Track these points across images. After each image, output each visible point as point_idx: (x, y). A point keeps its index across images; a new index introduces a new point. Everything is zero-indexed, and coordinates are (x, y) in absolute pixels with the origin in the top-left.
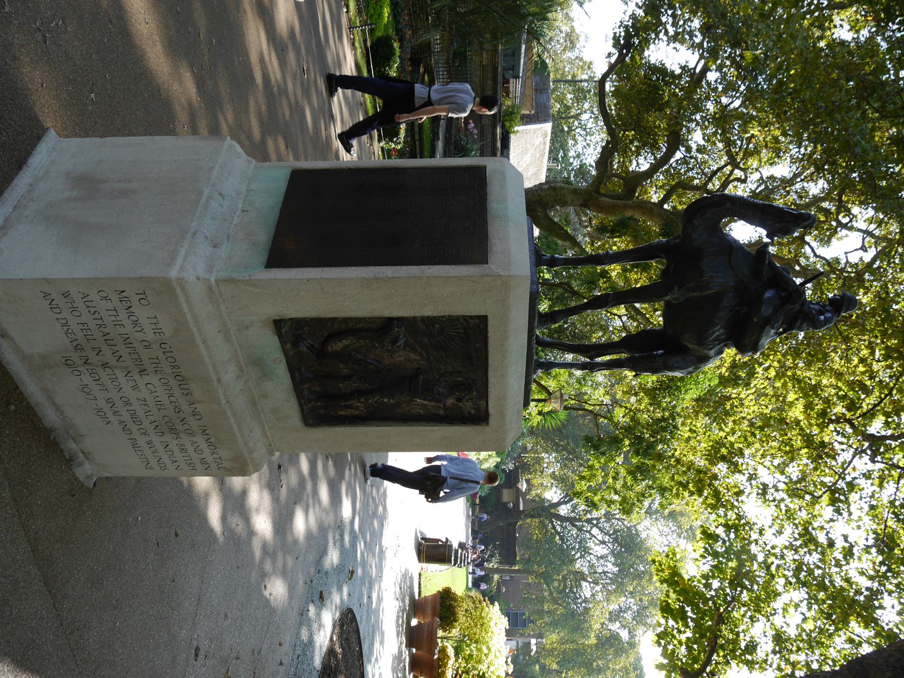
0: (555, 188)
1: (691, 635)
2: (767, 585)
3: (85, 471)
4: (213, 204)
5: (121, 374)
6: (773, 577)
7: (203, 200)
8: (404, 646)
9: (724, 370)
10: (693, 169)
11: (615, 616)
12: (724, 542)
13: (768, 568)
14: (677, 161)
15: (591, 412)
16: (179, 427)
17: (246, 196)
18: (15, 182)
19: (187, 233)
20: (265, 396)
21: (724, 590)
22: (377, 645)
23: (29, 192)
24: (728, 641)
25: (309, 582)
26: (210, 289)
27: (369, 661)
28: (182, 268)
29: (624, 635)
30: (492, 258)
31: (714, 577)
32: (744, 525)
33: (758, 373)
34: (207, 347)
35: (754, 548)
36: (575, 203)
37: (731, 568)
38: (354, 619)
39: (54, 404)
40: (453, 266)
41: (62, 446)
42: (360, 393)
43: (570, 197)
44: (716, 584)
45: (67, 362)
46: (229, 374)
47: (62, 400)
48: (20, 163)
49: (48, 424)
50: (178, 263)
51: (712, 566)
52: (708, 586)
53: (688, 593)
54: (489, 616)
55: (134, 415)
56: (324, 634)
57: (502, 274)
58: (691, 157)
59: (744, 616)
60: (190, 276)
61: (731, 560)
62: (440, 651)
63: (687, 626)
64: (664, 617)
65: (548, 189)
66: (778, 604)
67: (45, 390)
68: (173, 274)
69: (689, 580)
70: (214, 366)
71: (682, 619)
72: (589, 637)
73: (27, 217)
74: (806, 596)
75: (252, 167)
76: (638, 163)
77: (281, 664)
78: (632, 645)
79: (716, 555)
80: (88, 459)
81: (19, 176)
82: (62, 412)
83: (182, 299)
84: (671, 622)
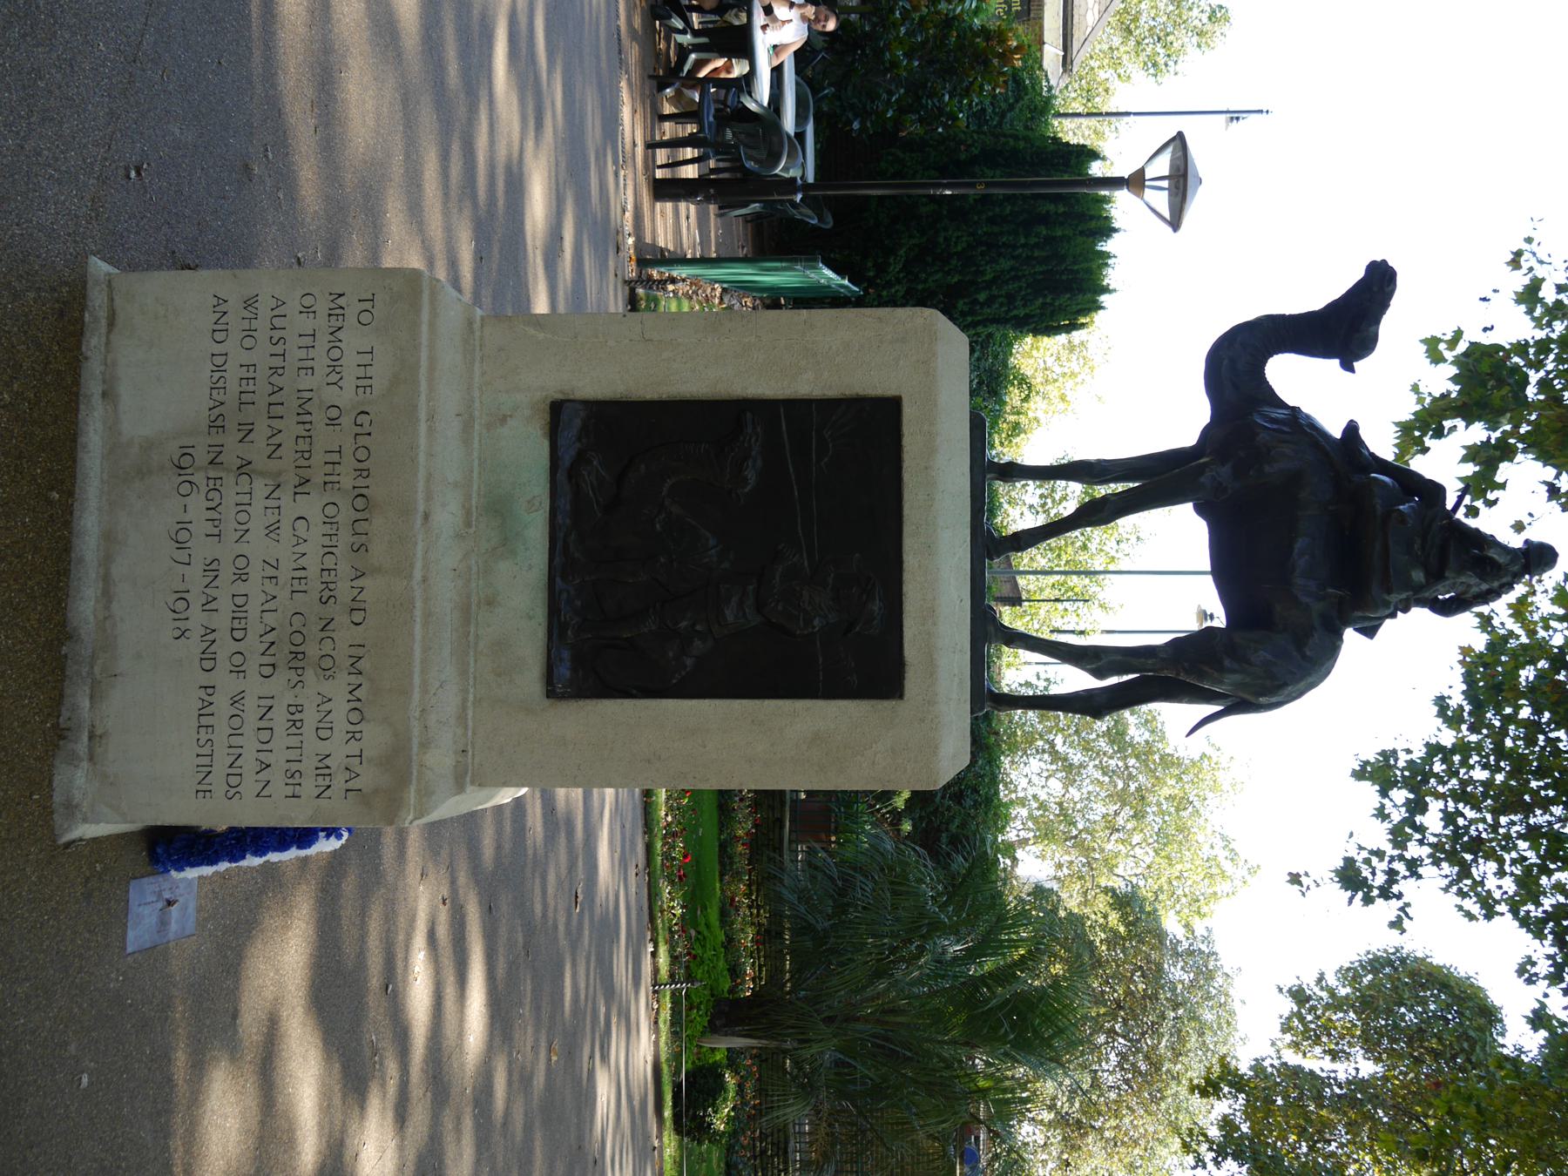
34: (431, 430)
46: (448, 515)
67: (109, 537)
80: (91, 758)
83: (425, 316)
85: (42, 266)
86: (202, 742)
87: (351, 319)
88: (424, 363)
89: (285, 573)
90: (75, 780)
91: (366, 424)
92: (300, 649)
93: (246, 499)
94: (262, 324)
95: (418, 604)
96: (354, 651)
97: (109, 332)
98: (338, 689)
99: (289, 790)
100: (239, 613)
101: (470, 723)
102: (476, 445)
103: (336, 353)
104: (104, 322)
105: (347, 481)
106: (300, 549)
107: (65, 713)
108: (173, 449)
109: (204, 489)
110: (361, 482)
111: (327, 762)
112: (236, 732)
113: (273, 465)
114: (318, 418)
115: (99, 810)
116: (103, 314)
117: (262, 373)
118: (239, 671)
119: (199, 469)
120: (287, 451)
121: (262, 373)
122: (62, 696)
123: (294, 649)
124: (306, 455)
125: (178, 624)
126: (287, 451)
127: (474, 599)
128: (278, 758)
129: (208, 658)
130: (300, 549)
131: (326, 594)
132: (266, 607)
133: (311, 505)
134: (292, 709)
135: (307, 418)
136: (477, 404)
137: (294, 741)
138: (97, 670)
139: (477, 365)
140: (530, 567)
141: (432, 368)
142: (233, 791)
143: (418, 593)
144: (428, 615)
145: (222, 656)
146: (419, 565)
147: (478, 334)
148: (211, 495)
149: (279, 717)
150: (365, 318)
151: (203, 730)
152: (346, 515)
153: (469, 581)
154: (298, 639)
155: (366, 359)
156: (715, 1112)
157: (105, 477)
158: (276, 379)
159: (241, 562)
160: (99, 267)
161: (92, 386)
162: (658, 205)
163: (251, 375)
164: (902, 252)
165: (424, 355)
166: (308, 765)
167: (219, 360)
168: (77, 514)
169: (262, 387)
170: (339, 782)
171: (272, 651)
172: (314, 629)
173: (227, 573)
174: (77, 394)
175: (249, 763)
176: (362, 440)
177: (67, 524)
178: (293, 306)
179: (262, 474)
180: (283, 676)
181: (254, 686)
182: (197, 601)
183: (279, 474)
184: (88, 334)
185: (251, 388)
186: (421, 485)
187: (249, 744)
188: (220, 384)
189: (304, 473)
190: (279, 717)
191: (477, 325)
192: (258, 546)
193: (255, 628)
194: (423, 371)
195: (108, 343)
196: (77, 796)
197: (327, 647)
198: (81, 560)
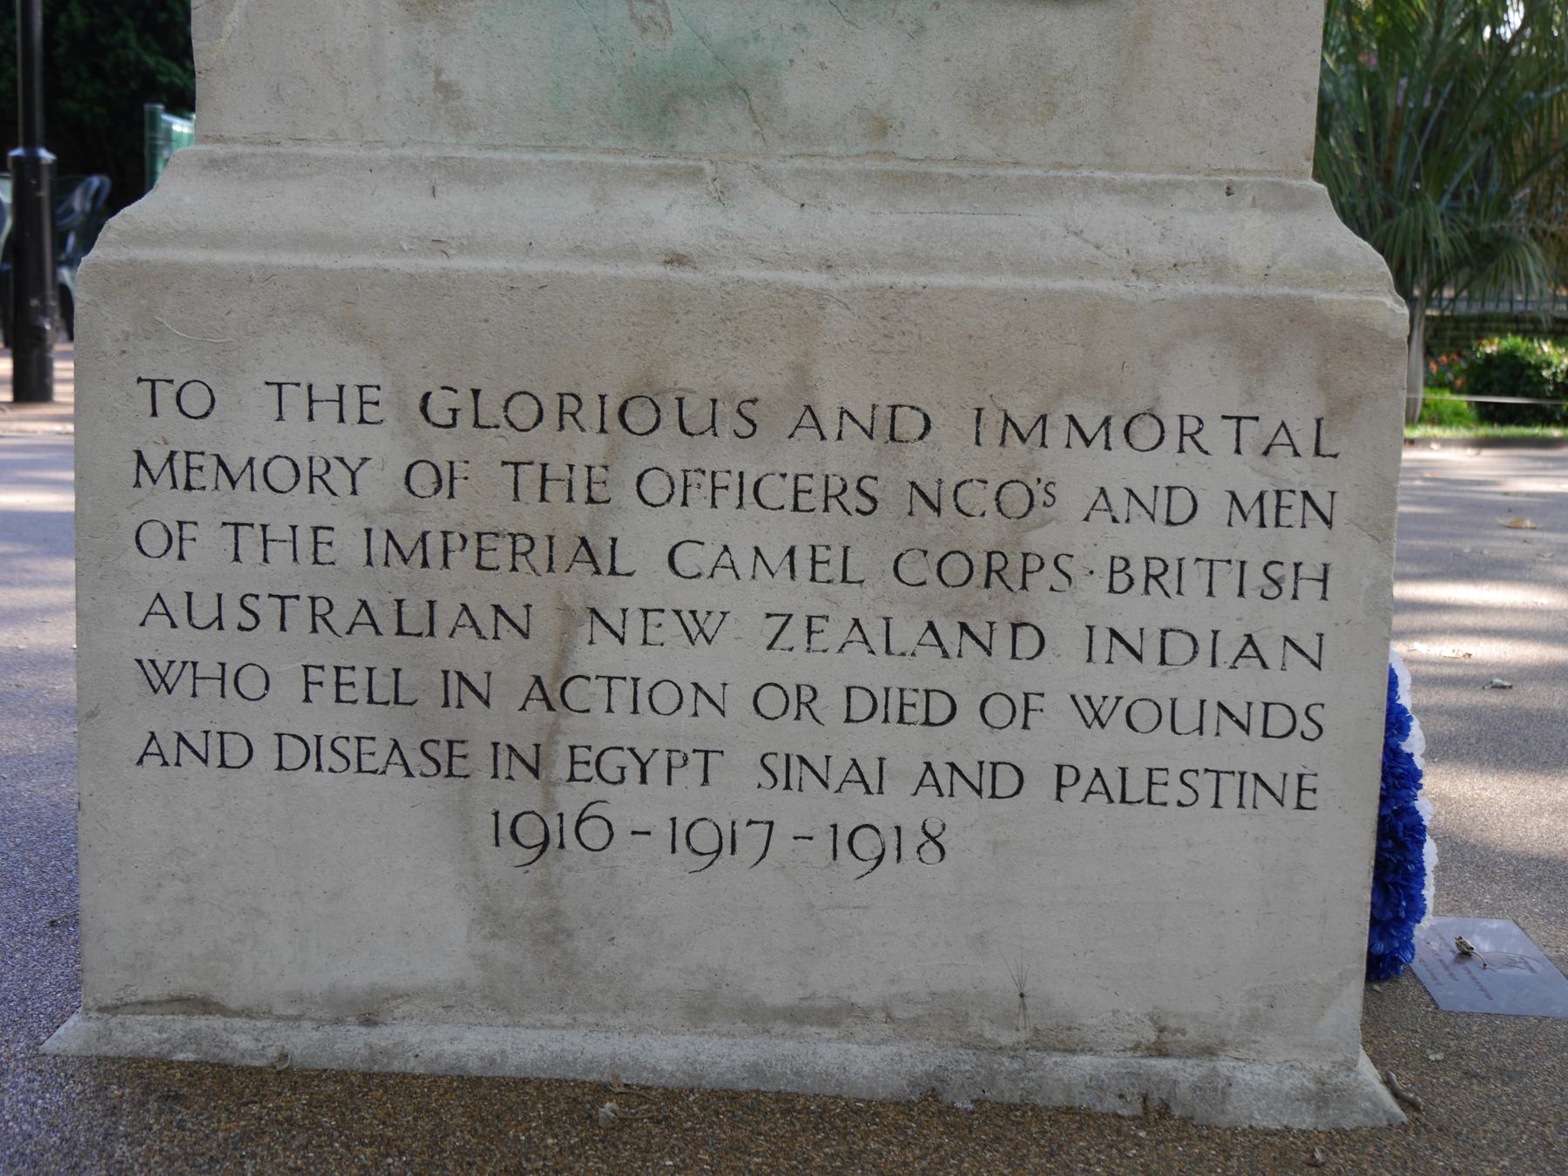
34: (469, 246)
46: (675, 217)
67: (701, 1011)
85: (53, 1127)
86: (1188, 797)
87: (199, 435)
88: (307, 259)
89: (801, 597)
90: (1264, 1083)
91: (453, 400)
92: (980, 562)
93: (623, 690)
94: (210, 650)
95: (885, 278)
96: (991, 434)
97: (223, 1011)
98: (1078, 472)
99: (1309, 590)
100: (887, 707)
101: (1165, 177)
102: (507, 156)
103: (281, 474)
104: (200, 1022)
105: (587, 447)
106: (744, 561)
107: (1111, 1103)
108: (502, 861)
109: (597, 789)
110: (590, 415)
111: (1248, 500)
112: (1168, 716)
113: (545, 623)
114: (436, 515)
115: (1303, 1053)
116: (179, 1024)
117: (326, 650)
118: (1025, 709)
119: (549, 798)
120: (511, 590)
121: (326, 650)
122: (1069, 1110)
123: (978, 578)
124: (523, 545)
125: (909, 850)
126: (511, 590)
127: (873, 165)
128: (1232, 616)
129: (992, 781)
130: (744, 561)
131: (853, 499)
132: (878, 643)
133: (642, 534)
134: (1121, 581)
135: (435, 543)
136: (408, 152)
137: (1195, 579)
138: (1007, 1038)
139: (313, 151)
140: (799, 28)
141: (322, 242)
142: (1304, 724)
143: (858, 279)
144: (911, 259)
145: (989, 747)
146: (792, 277)
147: (238, 149)
148: (611, 773)
149: (1138, 613)
150: (195, 400)
151: (1159, 793)
152: (668, 452)
153: (828, 175)
154: (956, 568)
155: (295, 400)
156: (1549, 365)
157: (560, 1019)
158: (340, 620)
159: (771, 701)
160: (71, 1035)
161: (351, 1045)
162: (57, 398)
163: (329, 677)
164: (151, 61)
165: (285, 259)
166: (1253, 544)
167: (294, 752)
168: (647, 1078)
169: (361, 650)
170: (1296, 472)
171: (981, 630)
172: (935, 530)
173: (794, 736)
174: (367, 1076)
175: (1242, 686)
176: (491, 410)
177: (672, 1095)
178: (167, 576)
179: (564, 655)
180: (1040, 604)
181: (1062, 673)
182: (854, 807)
183: (566, 610)
184: (227, 1055)
185: (361, 677)
186: (598, 269)
187: (1194, 683)
188: (350, 750)
189: (565, 549)
190: (1138, 613)
191: (220, 150)
192: (735, 662)
193: (928, 669)
194: (327, 261)
195: (247, 1013)
196: (1295, 1081)
197: (978, 498)
198: (755, 1070)
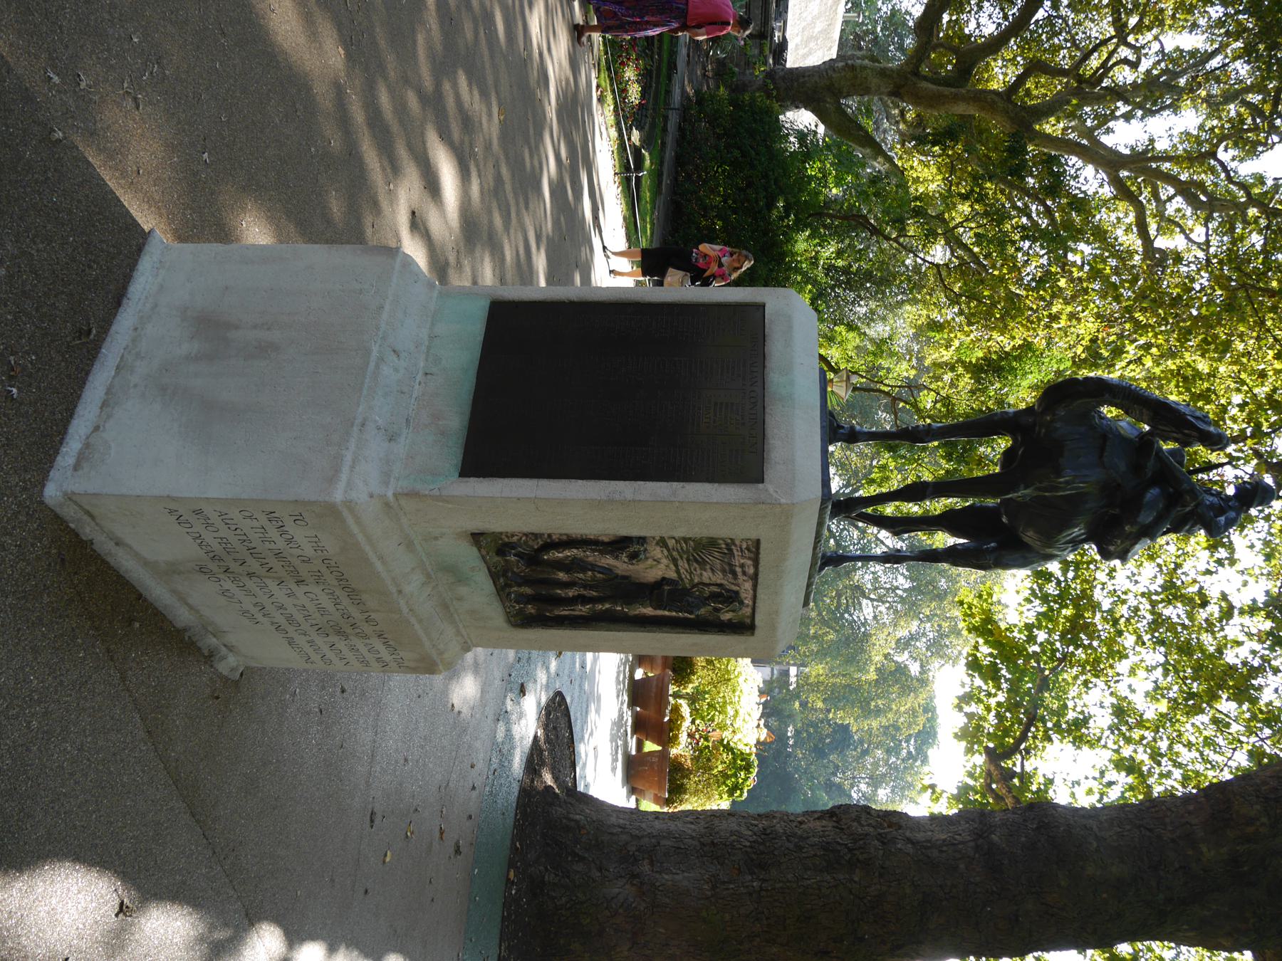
0: (853, 68)
1: (1003, 700)
2: (1110, 643)
3: (228, 665)
4: (386, 370)
5: (272, 585)
6: (1120, 633)
7: (372, 365)
8: (625, 706)
9: (1079, 350)
10: (1060, 34)
11: (903, 644)
12: (1059, 583)
13: (1115, 622)
14: (1037, 21)
15: (887, 394)
16: (349, 630)
17: (429, 348)
18: (114, 328)
19: (352, 425)
20: (460, 599)
21: (1052, 644)
22: (592, 715)
23: (134, 341)
24: (1052, 713)
25: (506, 677)
26: (387, 505)
27: (582, 738)
28: (350, 486)
29: (914, 668)
30: (773, 472)
31: (1039, 628)
32: (1089, 563)
33: (1127, 352)
34: (384, 563)
35: (1098, 594)
36: (882, 89)
37: (1065, 617)
38: (563, 698)
39: (187, 604)
40: (716, 485)
41: (199, 644)
42: (583, 600)
43: (874, 82)
44: (1042, 636)
45: (202, 570)
46: (413, 585)
47: (197, 603)
48: (118, 299)
49: (179, 624)
50: (344, 476)
51: (1039, 614)
52: (1031, 639)
53: (1007, 649)
54: (738, 669)
55: (290, 619)
56: (527, 724)
57: (783, 501)
58: (1059, 17)
59: (1076, 678)
60: (360, 495)
61: (1066, 606)
62: (671, 711)
63: (999, 688)
64: (969, 675)
65: (843, 69)
66: (1123, 666)
67: (174, 591)
68: (338, 496)
69: (1007, 629)
70: (393, 579)
71: (993, 679)
72: (868, 672)
73: (135, 386)
74: (1162, 659)
75: (435, 294)
76: (978, 24)
77: (474, 788)
78: (923, 681)
79: (1045, 599)
81: (118, 317)
82: (197, 611)
84: (978, 682)
